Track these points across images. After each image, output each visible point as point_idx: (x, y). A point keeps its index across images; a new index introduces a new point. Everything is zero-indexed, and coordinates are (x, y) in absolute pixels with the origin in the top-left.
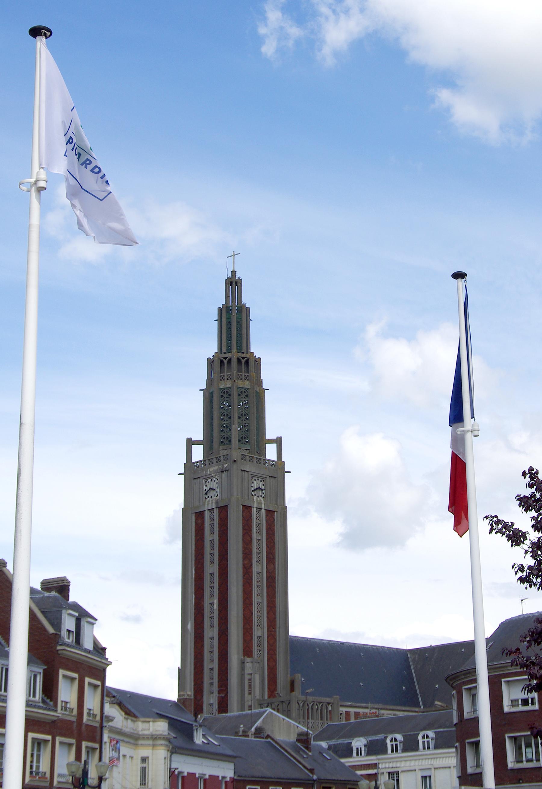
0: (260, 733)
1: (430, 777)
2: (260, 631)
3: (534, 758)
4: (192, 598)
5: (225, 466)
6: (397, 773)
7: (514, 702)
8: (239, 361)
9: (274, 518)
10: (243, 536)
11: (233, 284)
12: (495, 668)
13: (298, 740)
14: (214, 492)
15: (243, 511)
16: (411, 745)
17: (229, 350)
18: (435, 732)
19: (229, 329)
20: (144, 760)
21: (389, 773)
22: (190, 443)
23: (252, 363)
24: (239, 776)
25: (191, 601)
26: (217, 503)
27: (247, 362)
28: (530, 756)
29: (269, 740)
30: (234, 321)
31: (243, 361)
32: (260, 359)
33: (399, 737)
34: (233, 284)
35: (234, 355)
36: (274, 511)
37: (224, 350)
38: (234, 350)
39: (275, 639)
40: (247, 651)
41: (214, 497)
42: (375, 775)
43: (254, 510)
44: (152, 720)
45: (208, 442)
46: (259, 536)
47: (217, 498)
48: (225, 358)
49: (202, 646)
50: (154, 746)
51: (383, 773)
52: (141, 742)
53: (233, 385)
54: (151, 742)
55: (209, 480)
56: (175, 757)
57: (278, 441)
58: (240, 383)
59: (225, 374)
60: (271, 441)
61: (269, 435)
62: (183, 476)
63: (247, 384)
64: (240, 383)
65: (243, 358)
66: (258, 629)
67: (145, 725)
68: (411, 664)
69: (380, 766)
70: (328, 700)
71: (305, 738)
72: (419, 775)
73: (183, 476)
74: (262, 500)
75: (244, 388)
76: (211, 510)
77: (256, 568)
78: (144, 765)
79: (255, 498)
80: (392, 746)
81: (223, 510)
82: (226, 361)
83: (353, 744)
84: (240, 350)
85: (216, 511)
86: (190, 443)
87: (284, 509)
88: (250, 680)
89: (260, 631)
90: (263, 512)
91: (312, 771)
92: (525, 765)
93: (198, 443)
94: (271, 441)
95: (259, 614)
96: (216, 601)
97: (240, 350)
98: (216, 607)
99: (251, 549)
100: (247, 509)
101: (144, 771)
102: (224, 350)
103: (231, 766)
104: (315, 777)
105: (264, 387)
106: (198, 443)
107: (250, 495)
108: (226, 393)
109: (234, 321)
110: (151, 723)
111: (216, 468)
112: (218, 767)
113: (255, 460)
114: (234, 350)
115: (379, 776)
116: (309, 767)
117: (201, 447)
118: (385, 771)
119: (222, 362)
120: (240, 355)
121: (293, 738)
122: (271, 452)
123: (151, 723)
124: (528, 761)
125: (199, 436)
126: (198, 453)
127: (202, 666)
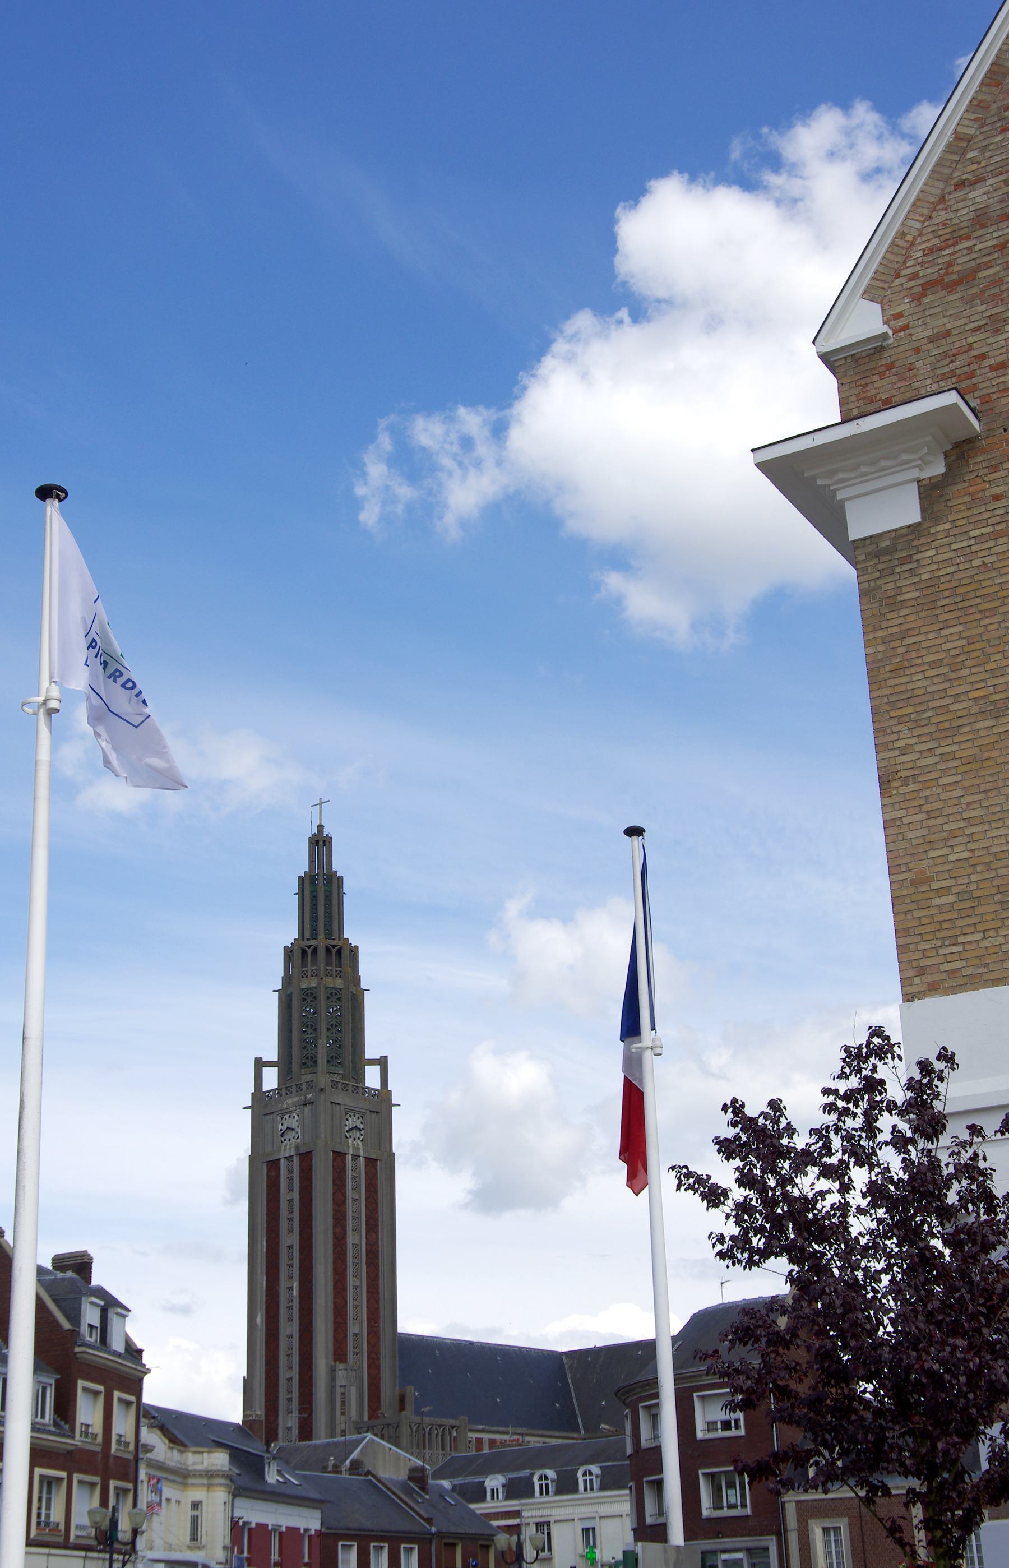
0: (357, 1468)
1: (594, 1529)
2: (357, 1327)
3: (739, 1503)
4: (262, 1280)
5: (309, 1096)
6: (548, 1524)
7: (711, 1426)
8: (328, 950)
9: (376, 1169)
10: (334, 1194)
11: (320, 843)
12: (684, 1378)
13: (410, 1478)
14: (293, 1133)
15: (334, 1160)
16: (567, 1485)
17: (314, 935)
18: (601, 1467)
19: (314, 906)
20: (196, 1505)
21: (537, 1524)
22: (260, 1064)
23: (345, 954)
24: (328, 1528)
25: (261, 1284)
26: (297, 1147)
27: (339, 952)
28: (733, 1501)
29: (370, 1477)
30: (321, 895)
31: (334, 951)
32: (357, 947)
33: (551, 1474)
34: (320, 843)
35: (321, 942)
36: (376, 1160)
37: (307, 935)
38: (321, 936)
39: (379, 1337)
40: (339, 1354)
41: (293, 1140)
42: (518, 1526)
43: (349, 1158)
44: (206, 1449)
45: (285, 1064)
46: (355, 1195)
47: (298, 1141)
48: (309, 947)
49: (277, 1346)
50: (209, 1486)
51: (528, 1524)
52: (191, 1481)
53: (319, 984)
54: (205, 1481)
55: (287, 1116)
56: (239, 1502)
57: (383, 1062)
58: (329, 982)
59: (309, 968)
60: (372, 1062)
61: (371, 1052)
62: (250, 1110)
63: (339, 983)
64: (329, 982)
65: (334, 946)
66: (354, 1324)
67: (198, 1458)
68: (568, 1372)
69: (525, 1514)
70: (452, 1422)
71: (420, 1475)
72: (579, 1526)
73: (250, 1110)
74: (360, 1144)
75: (335, 989)
76: (289, 1158)
77: (351, 1239)
78: (196, 1513)
79: (350, 1141)
80: (541, 1486)
81: (306, 1158)
82: (309, 951)
83: (486, 1484)
84: (329, 935)
85: (296, 1160)
86: (260, 1064)
87: (391, 1156)
88: (343, 1394)
89: (357, 1327)
90: (362, 1160)
91: (429, 1521)
92: (726, 1512)
93: (270, 1064)
94: (372, 1062)
95: (356, 1303)
96: (296, 1285)
97: (329, 935)
98: (295, 1292)
99: (345, 1212)
100: (339, 1156)
101: (195, 1521)
102: (307, 935)
103: (317, 1514)
104: (434, 1529)
105: (363, 986)
106: (270, 1064)
107: (343, 1136)
108: (309, 996)
109: (321, 895)
110: (205, 1455)
111: (295, 1099)
112: (299, 1515)
113: (350, 1089)
114: (321, 936)
115: (523, 1528)
116: (426, 1516)
117: (275, 1070)
118: (527, 1521)
119: (304, 952)
120: (329, 942)
121: (403, 1475)
122: (372, 1078)
123: (205, 1455)
124: (731, 1507)
125: (272, 1054)
126: (271, 1079)
127: (277, 1375)
